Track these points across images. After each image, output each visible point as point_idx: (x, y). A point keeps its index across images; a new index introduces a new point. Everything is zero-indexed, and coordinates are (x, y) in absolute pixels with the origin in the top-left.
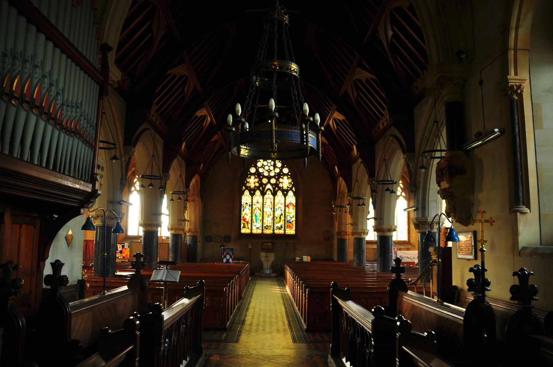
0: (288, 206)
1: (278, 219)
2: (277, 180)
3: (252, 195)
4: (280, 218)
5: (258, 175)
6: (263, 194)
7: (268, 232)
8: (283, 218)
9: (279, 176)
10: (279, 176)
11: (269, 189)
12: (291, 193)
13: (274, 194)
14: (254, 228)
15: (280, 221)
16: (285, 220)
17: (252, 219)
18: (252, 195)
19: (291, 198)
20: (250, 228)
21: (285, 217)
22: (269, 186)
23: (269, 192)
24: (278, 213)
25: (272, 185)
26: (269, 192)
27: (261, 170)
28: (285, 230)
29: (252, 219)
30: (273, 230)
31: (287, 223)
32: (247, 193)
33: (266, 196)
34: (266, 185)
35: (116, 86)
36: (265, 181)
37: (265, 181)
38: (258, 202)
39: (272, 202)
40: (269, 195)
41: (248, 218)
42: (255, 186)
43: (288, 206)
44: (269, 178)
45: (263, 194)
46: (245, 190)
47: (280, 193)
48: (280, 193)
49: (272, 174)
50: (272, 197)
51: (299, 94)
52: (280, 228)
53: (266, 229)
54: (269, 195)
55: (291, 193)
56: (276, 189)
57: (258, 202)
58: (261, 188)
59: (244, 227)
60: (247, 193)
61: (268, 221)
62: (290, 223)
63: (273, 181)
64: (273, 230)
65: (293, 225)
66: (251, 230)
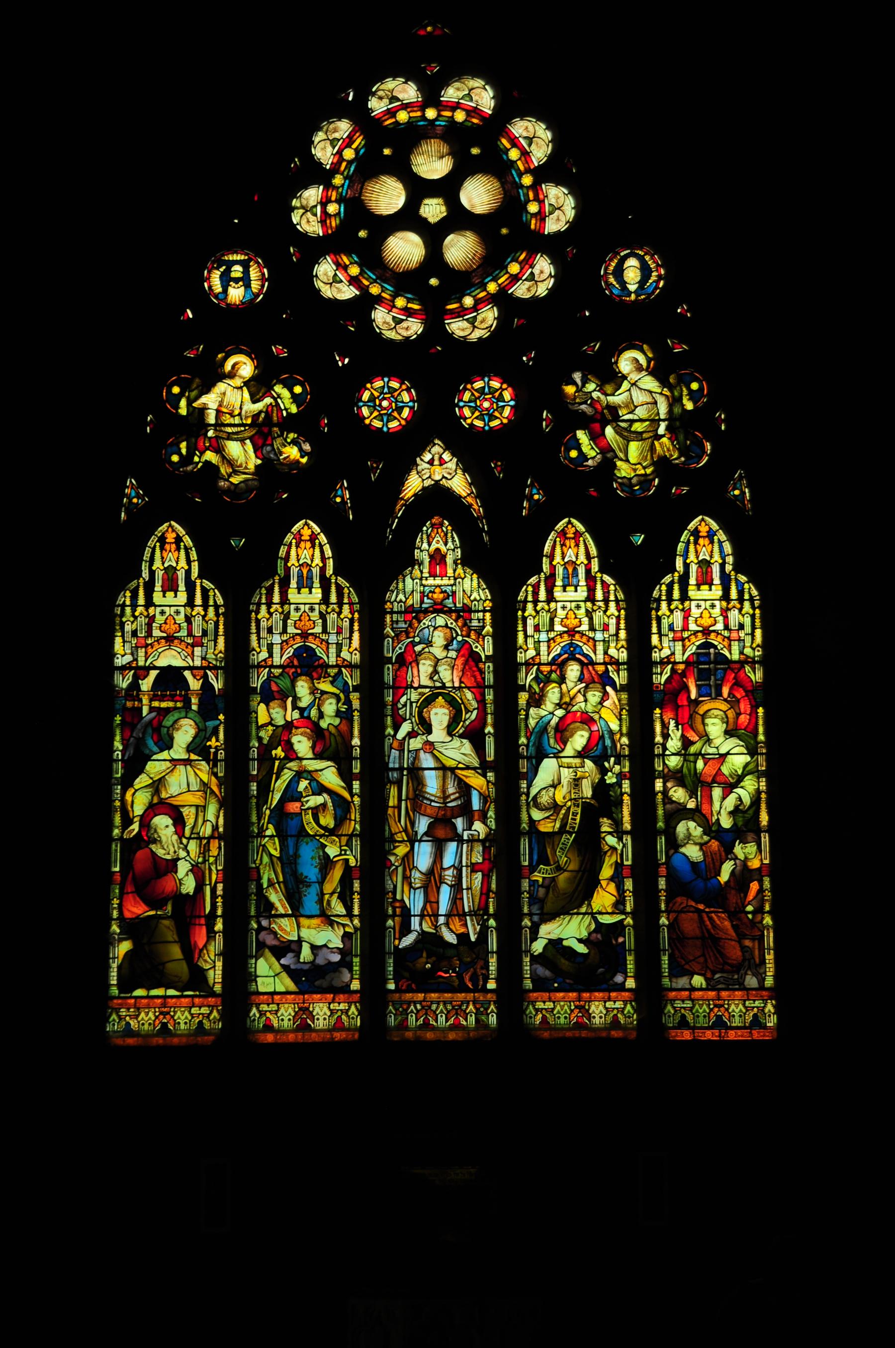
0: (673, 695)
1: (565, 856)
2: (538, 391)
3: (241, 572)
4: (589, 847)
5: (307, 341)
6: (371, 561)
7: (442, 1015)
8: (617, 845)
9: (559, 341)
10: (559, 341)
11: (437, 499)
12: (706, 545)
13: (507, 560)
14: (268, 975)
15: (587, 884)
16: (644, 869)
17: (239, 874)
18: (241, 572)
19: (711, 606)
20: (215, 976)
21: (644, 832)
22: (438, 469)
23: (439, 541)
24: (557, 780)
25: (469, 448)
26: (439, 541)
27: (333, 281)
28: (650, 996)
29: (239, 874)
30: (511, 998)
31: (680, 915)
32: (172, 553)
33: (409, 588)
34: (404, 449)
35: (310, 755)
36: (384, 403)
37: (384, 403)
38: (307, 663)
39: (486, 648)
40: (440, 575)
41: (185, 854)
42: (270, 470)
43: (673, 695)
44: (436, 366)
45: (371, 561)
46: (144, 525)
47: (571, 549)
48: (571, 549)
49: (475, 324)
50: (471, 588)
51: (715, 955)
52: (584, 972)
53: (426, 982)
54: (440, 575)
55: (706, 545)
56: (522, 503)
57: (307, 663)
58: (343, 495)
59: (144, 970)
60: (172, 553)
61: (440, 883)
62: (719, 897)
63: (489, 403)
64: (511, 998)
65: (749, 929)
66: (239, 989)
